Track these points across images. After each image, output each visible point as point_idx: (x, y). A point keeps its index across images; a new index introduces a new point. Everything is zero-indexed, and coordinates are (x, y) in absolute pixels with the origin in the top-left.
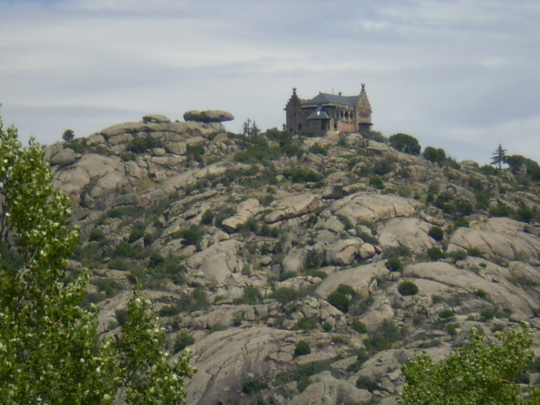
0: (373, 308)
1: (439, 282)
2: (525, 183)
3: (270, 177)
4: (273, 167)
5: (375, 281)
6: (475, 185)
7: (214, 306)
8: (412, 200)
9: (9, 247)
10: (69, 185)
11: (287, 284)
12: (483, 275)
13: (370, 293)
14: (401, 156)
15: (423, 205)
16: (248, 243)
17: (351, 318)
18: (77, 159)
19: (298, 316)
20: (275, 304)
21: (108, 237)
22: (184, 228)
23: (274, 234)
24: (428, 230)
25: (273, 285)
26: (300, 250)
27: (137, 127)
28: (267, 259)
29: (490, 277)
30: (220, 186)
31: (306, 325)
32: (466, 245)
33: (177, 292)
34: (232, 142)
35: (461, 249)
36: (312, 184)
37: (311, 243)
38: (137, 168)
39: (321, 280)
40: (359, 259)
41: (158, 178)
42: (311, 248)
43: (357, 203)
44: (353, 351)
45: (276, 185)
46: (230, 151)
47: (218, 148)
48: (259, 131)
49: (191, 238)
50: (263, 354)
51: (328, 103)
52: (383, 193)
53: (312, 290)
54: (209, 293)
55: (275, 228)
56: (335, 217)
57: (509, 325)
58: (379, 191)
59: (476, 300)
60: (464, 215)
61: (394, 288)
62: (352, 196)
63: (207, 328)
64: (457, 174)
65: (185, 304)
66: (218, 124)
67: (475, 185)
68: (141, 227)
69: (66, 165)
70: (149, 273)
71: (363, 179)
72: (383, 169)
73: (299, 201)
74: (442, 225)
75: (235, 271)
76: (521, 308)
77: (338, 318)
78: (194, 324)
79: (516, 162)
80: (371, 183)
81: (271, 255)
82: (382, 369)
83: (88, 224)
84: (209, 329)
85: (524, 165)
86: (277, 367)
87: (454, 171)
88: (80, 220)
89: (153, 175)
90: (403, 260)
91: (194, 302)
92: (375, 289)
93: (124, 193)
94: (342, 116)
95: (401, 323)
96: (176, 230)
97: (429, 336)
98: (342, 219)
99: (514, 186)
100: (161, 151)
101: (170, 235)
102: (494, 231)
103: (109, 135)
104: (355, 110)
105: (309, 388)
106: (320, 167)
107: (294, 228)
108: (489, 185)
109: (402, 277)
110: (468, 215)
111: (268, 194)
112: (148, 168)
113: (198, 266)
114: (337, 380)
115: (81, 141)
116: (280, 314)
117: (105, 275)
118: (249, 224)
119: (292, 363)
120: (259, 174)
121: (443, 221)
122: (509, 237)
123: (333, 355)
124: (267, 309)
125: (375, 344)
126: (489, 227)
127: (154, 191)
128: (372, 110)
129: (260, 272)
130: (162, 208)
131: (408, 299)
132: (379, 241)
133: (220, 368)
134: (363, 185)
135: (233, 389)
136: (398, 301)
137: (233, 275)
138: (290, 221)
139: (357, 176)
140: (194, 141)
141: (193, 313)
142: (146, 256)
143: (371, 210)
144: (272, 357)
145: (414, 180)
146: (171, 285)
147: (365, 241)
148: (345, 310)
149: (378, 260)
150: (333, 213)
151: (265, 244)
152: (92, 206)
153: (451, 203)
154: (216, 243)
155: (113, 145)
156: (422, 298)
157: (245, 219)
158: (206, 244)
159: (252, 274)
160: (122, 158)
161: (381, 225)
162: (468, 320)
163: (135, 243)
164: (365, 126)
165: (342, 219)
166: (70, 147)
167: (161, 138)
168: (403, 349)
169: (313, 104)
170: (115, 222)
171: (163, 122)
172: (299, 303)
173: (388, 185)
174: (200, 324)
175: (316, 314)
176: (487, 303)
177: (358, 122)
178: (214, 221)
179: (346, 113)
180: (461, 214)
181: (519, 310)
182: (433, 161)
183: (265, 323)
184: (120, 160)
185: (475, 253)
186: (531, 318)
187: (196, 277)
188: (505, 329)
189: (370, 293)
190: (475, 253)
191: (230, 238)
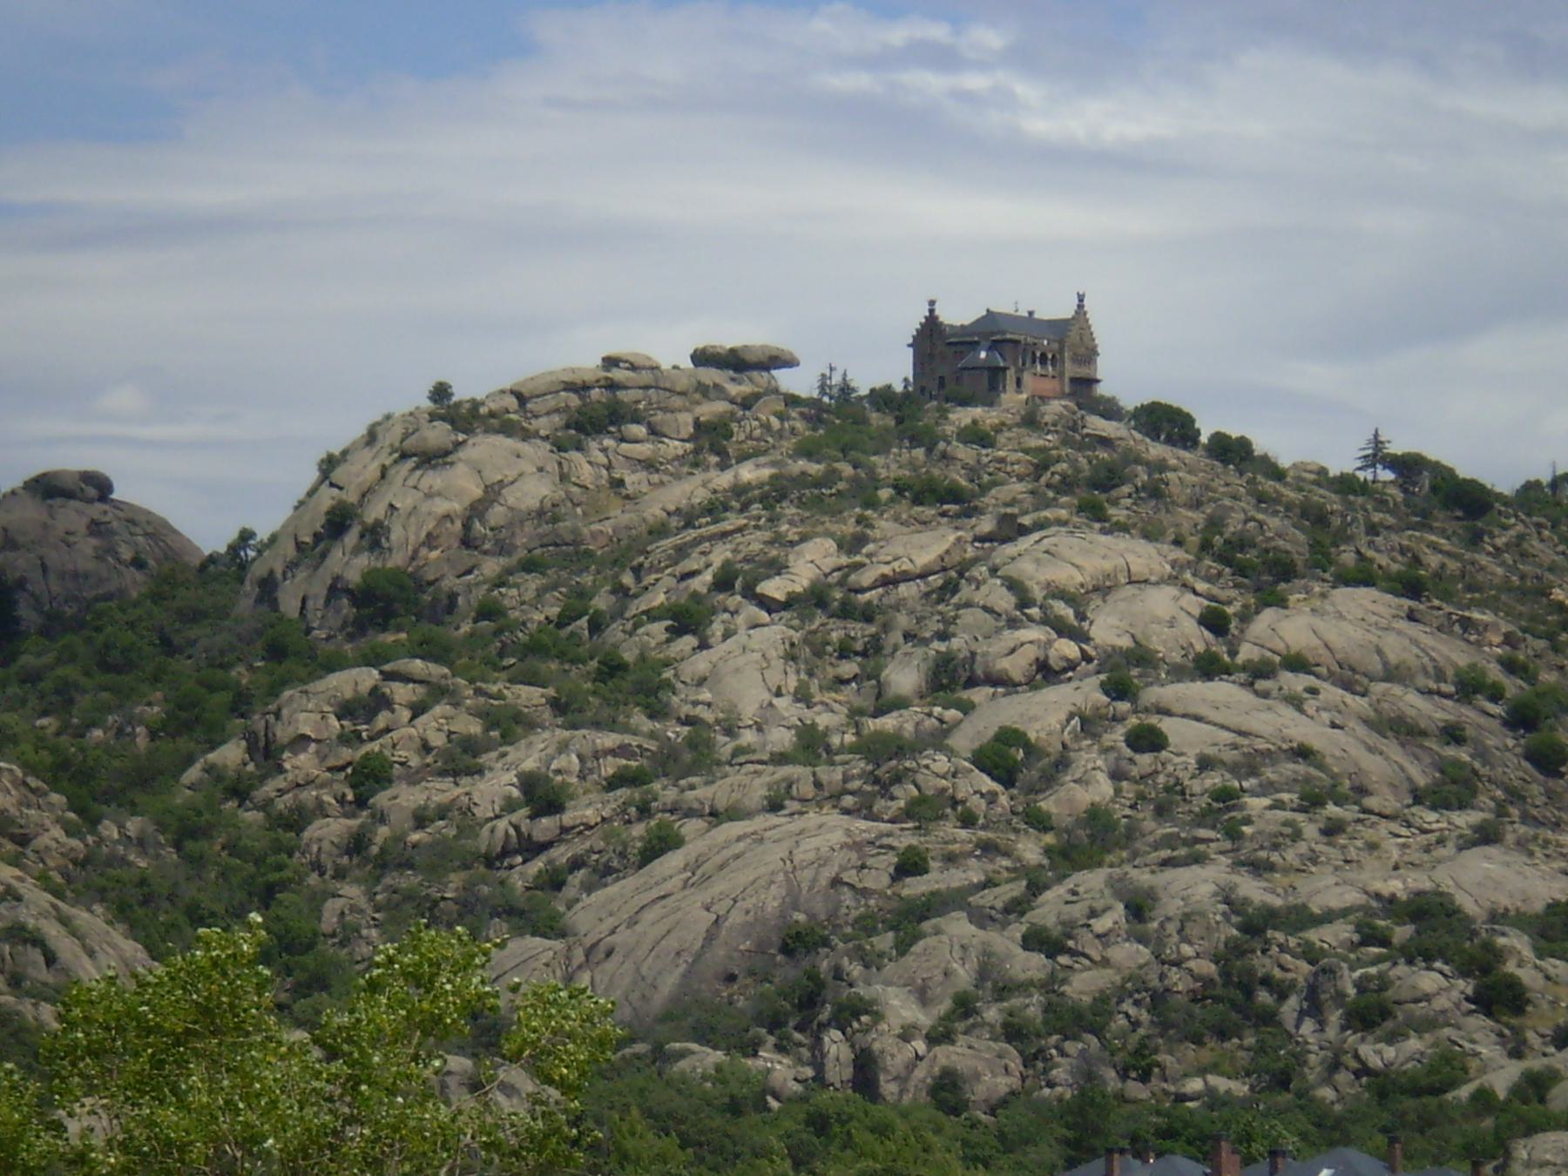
0: (1069, 778)
1: (1215, 724)
2: (1425, 514)
3: (864, 493)
4: (871, 472)
5: (1076, 721)
6: (1315, 517)
7: (727, 768)
8: (1165, 548)
9: (308, 631)
10: (437, 500)
11: (888, 722)
12: (1311, 711)
13: (1064, 746)
14: (1156, 450)
15: (1191, 557)
16: (811, 632)
17: (1021, 798)
18: (458, 445)
19: (905, 793)
20: (860, 766)
21: (514, 614)
22: (674, 598)
23: (867, 615)
24: (1197, 612)
25: (857, 725)
26: (920, 651)
27: (589, 378)
28: (849, 668)
29: (1326, 717)
30: (756, 509)
31: (922, 812)
32: (1280, 646)
33: (652, 735)
34: (794, 414)
35: (1269, 654)
36: (952, 508)
37: (943, 636)
38: (585, 467)
39: (959, 715)
40: (1046, 673)
41: (630, 489)
42: (942, 647)
43: (1047, 552)
44: (1019, 869)
45: (875, 510)
46: (787, 434)
47: (762, 426)
48: (854, 390)
49: (687, 620)
50: (828, 873)
51: (1004, 333)
52: (1103, 531)
53: (939, 739)
54: (721, 739)
55: (869, 603)
56: (998, 582)
57: (1359, 821)
58: (1097, 526)
59: (1291, 766)
60: (1277, 582)
61: (1116, 736)
62: (1036, 536)
63: (711, 814)
64: (1276, 491)
65: (668, 762)
66: (765, 374)
67: (1315, 517)
68: (583, 594)
69: (431, 459)
70: (594, 693)
71: (1064, 499)
72: (1108, 479)
73: (923, 545)
74: (1229, 603)
75: (778, 694)
76: (1392, 785)
77: (991, 798)
78: (685, 806)
79: (1408, 467)
80: (1080, 509)
81: (859, 659)
82: (1077, 911)
83: (477, 584)
84: (716, 816)
85: (1426, 473)
86: (858, 901)
87: (1269, 485)
88: (459, 577)
89: (620, 483)
90: (1140, 676)
91: (687, 757)
92: (1076, 738)
93: (555, 519)
94: (1034, 362)
95: (1128, 812)
96: (656, 603)
97: (1185, 842)
98: (1013, 585)
99: (1400, 519)
100: (639, 430)
101: (643, 612)
102: (1341, 616)
103: (527, 395)
104: (1063, 347)
105: (917, 948)
106: (973, 472)
107: (910, 602)
108: (1344, 517)
109: (1135, 712)
110: (1288, 581)
111: (858, 529)
112: (609, 467)
113: (701, 682)
114: (981, 933)
115: (467, 406)
116: (868, 788)
117: (499, 696)
118: (813, 592)
119: (889, 892)
120: (841, 486)
121: (1233, 593)
122: (1373, 629)
123: (976, 877)
124: (840, 777)
125: (1068, 857)
126: (1329, 608)
127: (620, 517)
128: (1099, 350)
129: (833, 695)
130: (629, 554)
131: (1145, 760)
132: (1092, 634)
133: (735, 901)
134: (1063, 513)
135: (761, 948)
136: (1124, 764)
137: (775, 701)
138: (902, 588)
139: (1051, 494)
140: (711, 409)
141: (683, 782)
142: (592, 658)
143: (1077, 567)
144: (846, 880)
145: (1173, 502)
146: (639, 719)
147: (1060, 634)
148: (1008, 781)
149: (1087, 675)
150: (994, 571)
151: (848, 635)
152: (487, 546)
153: (1251, 555)
154: (742, 630)
155: (536, 417)
156: (1177, 760)
157: (806, 583)
158: (719, 634)
159: (816, 700)
160: (553, 444)
161: (1096, 601)
162: (1271, 808)
163: (570, 628)
164: (1085, 384)
165: (1013, 585)
166: (443, 418)
167: (638, 402)
168: (1127, 868)
169: (973, 334)
170: (532, 583)
171: (644, 368)
172: (907, 764)
173: (1117, 514)
174: (696, 805)
175: (944, 790)
176: (1313, 771)
177: (1067, 376)
178: (738, 584)
179: (1043, 355)
180: (1270, 578)
181: (1386, 790)
182: (1225, 462)
183: (834, 807)
184: (549, 447)
185: (1297, 663)
186: (1409, 806)
187: (695, 703)
188: (1349, 829)
189: (1064, 746)
190: (1297, 663)
191: (773, 623)
